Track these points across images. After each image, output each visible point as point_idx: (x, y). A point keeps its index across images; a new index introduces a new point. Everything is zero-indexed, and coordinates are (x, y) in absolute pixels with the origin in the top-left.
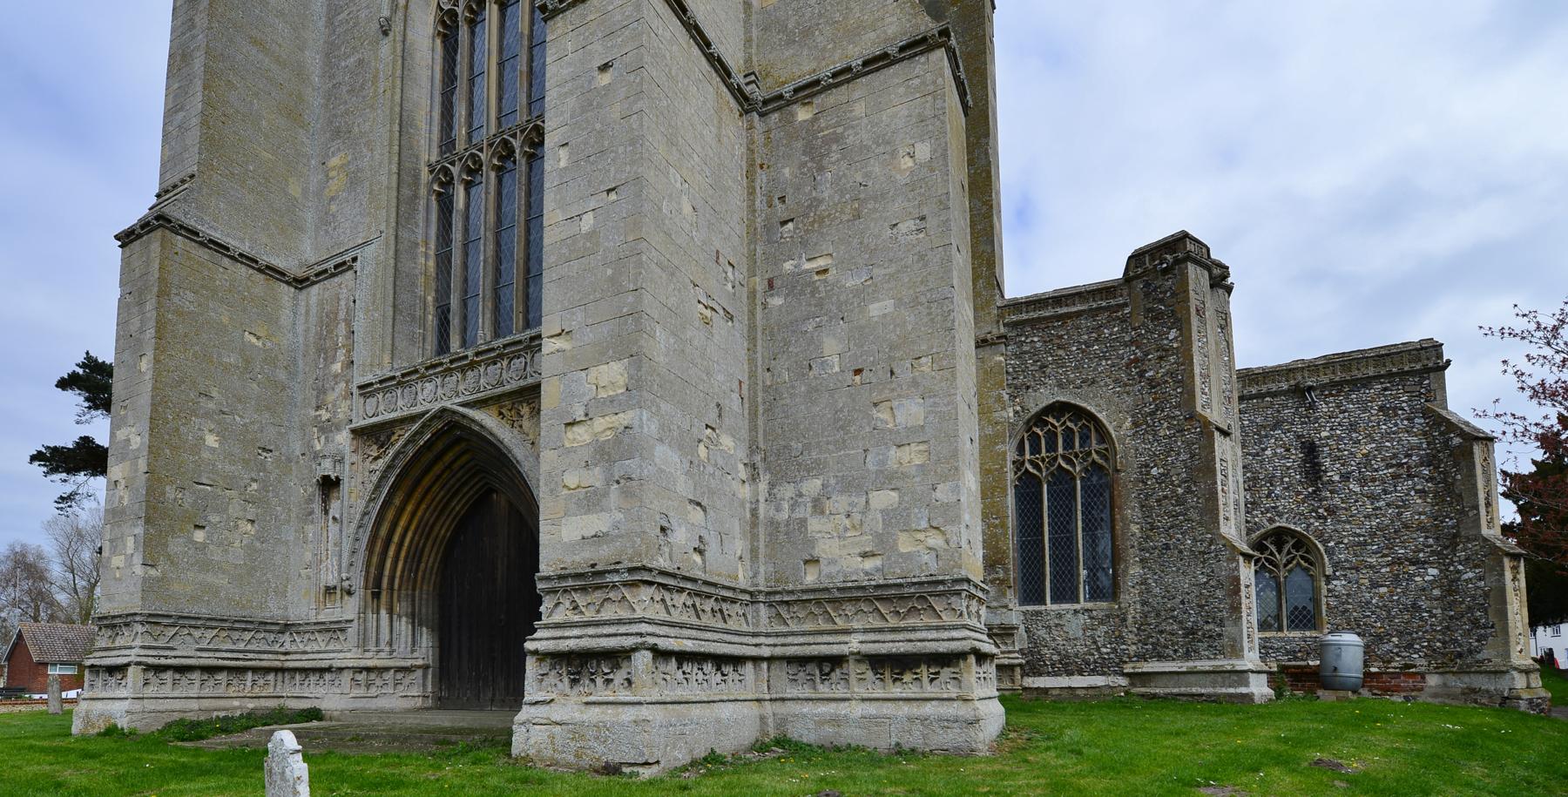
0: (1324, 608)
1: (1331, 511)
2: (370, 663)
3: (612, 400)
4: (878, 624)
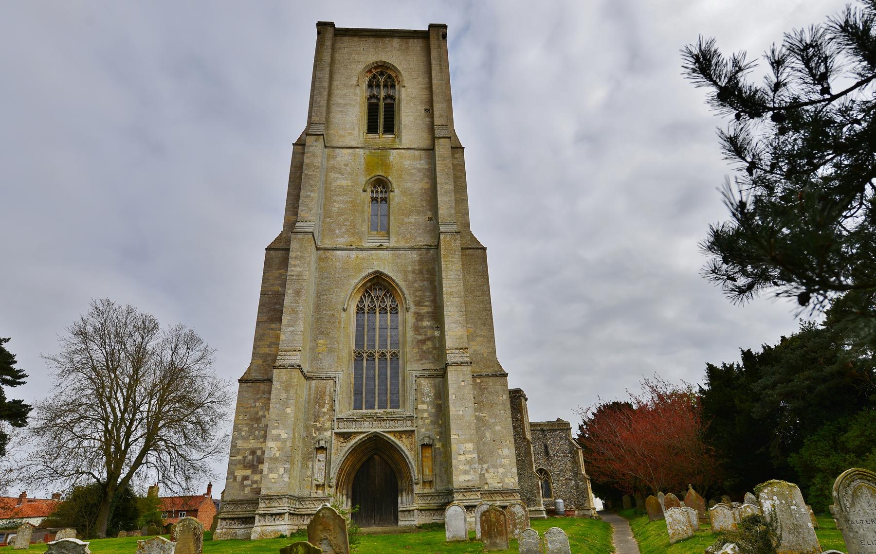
1: (552, 464)
4: (503, 499)
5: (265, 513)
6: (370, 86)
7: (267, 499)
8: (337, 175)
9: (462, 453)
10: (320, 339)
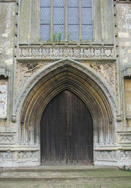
2: (24, 149)
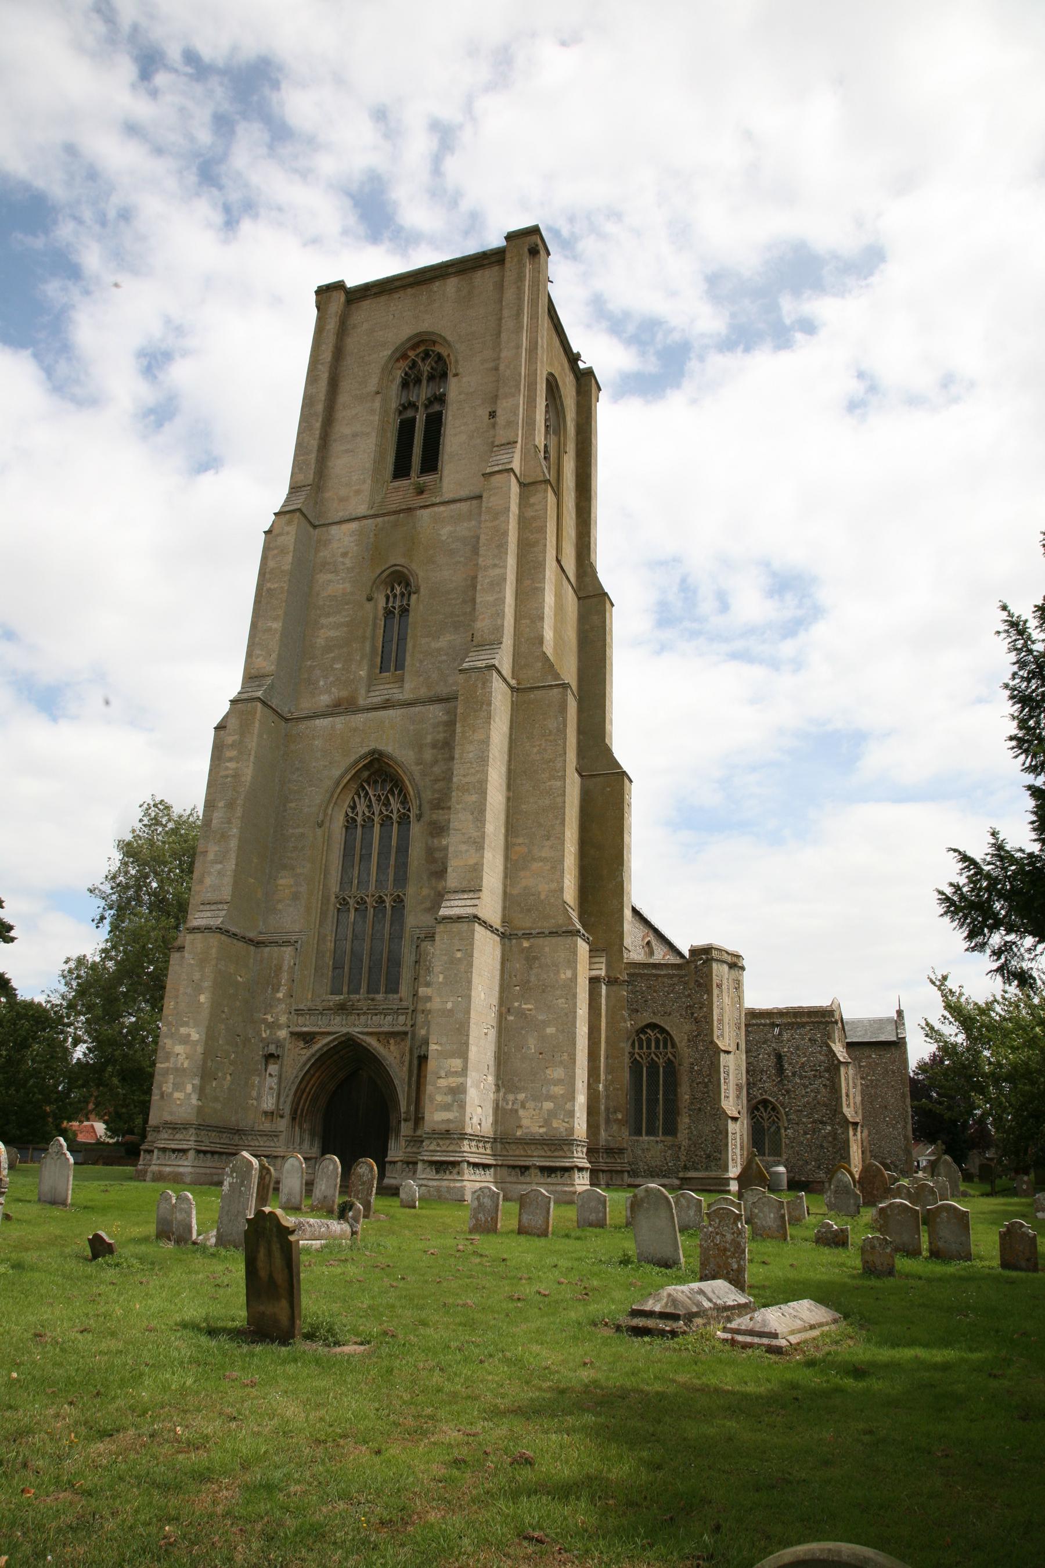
0: (784, 1144)
1: (788, 1091)
3: (456, 1072)
4: (543, 1154)
5: (164, 1148)
6: (405, 384)
7: (170, 1128)
8: (330, 576)
9: (443, 1074)
10: (281, 878)
